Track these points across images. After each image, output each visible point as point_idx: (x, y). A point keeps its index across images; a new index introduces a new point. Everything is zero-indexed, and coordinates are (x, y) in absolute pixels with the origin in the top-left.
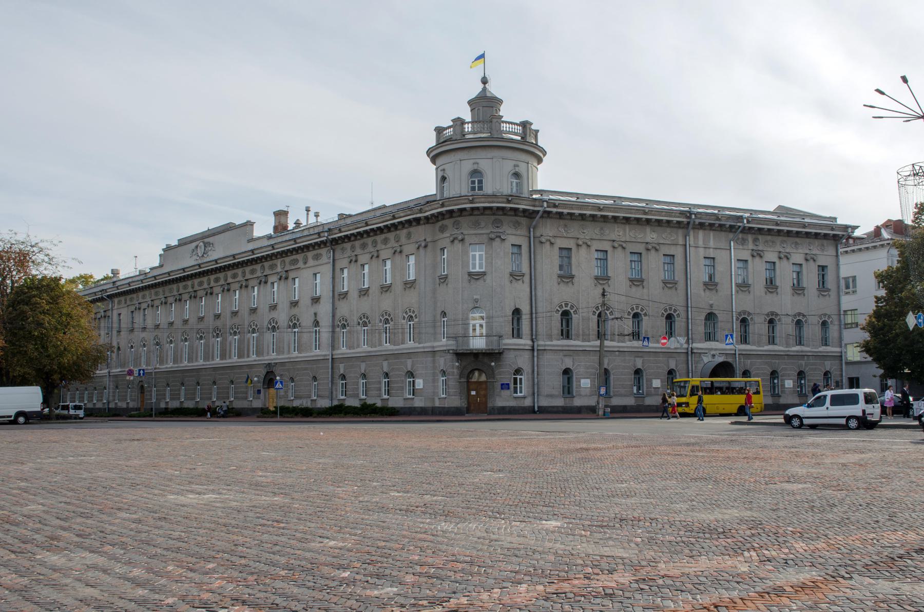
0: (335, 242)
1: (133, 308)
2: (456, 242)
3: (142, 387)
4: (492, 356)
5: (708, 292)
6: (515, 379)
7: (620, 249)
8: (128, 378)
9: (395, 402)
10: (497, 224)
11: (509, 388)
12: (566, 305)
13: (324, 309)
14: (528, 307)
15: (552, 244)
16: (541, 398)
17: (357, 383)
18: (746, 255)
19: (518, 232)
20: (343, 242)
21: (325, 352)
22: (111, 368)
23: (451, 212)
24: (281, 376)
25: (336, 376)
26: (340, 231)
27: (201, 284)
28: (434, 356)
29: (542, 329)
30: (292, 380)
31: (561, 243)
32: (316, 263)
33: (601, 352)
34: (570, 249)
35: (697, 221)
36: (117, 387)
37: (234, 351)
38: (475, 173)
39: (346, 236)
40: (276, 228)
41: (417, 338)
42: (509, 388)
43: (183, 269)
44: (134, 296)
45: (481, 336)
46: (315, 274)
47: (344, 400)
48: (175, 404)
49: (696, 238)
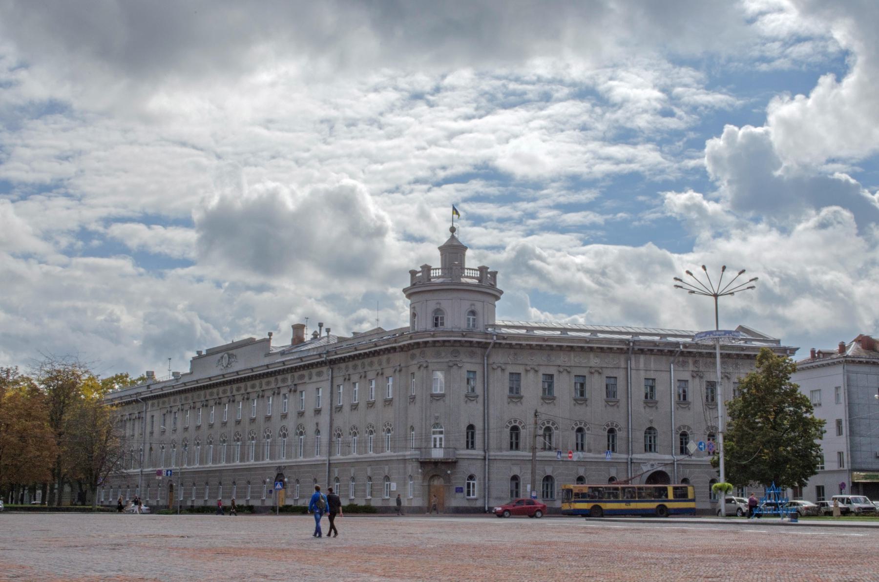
0: (332, 363)
1: (165, 411)
2: (422, 368)
3: (171, 486)
4: (451, 464)
5: (648, 409)
6: (469, 485)
7: (565, 373)
8: (157, 478)
9: (376, 502)
10: (456, 353)
11: (462, 492)
12: (515, 421)
13: (324, 419)
14: (481, 424)
15: (503, 370)
16: (491, 500)
17: (348, 486)
18: (686, 375)
19: (473, 361)
20: (339, 363)
21: (325, 458)
22: (143, 467)
23: (418, 344)
24: (289, 478)
25: (332, 479)
26: (336, 354)
27: (224, 392)
28: (405, 463)
29: (493, 443)
30: (298, 481)
31: (511, 369)
32: (319, 379)
33: (533, 461)
34: (519, 374)
35: (636, 348)
36: (148, 486)
37: (252, 454)
38: (438, 311)
39: (341, 358)
40: (293, 340)
41: (394, 449)
42: (462, 492)
43: (210, 378)
44: (166, 399)
45: (441, 447)
46: (318, 389)
47: (370, 500)
48: (199, 503)
49: (637, 362)
